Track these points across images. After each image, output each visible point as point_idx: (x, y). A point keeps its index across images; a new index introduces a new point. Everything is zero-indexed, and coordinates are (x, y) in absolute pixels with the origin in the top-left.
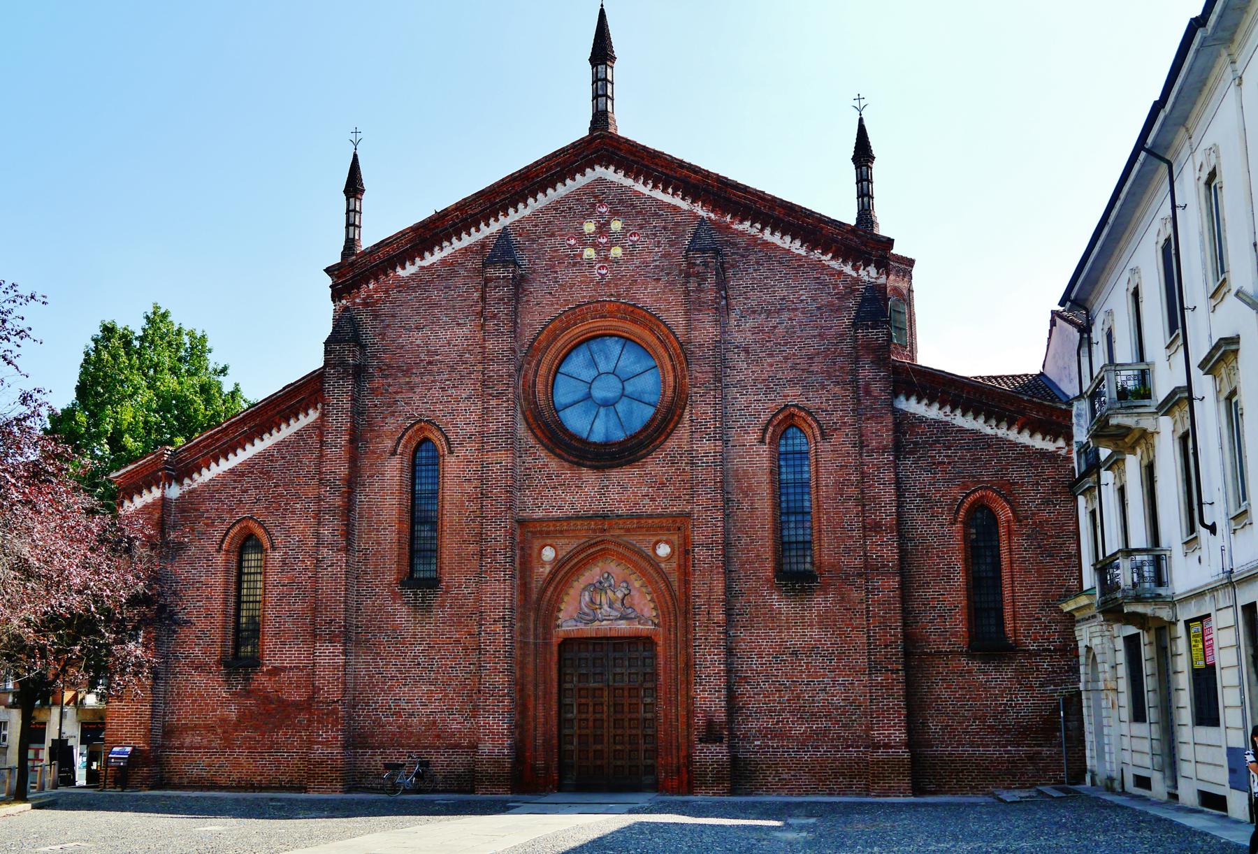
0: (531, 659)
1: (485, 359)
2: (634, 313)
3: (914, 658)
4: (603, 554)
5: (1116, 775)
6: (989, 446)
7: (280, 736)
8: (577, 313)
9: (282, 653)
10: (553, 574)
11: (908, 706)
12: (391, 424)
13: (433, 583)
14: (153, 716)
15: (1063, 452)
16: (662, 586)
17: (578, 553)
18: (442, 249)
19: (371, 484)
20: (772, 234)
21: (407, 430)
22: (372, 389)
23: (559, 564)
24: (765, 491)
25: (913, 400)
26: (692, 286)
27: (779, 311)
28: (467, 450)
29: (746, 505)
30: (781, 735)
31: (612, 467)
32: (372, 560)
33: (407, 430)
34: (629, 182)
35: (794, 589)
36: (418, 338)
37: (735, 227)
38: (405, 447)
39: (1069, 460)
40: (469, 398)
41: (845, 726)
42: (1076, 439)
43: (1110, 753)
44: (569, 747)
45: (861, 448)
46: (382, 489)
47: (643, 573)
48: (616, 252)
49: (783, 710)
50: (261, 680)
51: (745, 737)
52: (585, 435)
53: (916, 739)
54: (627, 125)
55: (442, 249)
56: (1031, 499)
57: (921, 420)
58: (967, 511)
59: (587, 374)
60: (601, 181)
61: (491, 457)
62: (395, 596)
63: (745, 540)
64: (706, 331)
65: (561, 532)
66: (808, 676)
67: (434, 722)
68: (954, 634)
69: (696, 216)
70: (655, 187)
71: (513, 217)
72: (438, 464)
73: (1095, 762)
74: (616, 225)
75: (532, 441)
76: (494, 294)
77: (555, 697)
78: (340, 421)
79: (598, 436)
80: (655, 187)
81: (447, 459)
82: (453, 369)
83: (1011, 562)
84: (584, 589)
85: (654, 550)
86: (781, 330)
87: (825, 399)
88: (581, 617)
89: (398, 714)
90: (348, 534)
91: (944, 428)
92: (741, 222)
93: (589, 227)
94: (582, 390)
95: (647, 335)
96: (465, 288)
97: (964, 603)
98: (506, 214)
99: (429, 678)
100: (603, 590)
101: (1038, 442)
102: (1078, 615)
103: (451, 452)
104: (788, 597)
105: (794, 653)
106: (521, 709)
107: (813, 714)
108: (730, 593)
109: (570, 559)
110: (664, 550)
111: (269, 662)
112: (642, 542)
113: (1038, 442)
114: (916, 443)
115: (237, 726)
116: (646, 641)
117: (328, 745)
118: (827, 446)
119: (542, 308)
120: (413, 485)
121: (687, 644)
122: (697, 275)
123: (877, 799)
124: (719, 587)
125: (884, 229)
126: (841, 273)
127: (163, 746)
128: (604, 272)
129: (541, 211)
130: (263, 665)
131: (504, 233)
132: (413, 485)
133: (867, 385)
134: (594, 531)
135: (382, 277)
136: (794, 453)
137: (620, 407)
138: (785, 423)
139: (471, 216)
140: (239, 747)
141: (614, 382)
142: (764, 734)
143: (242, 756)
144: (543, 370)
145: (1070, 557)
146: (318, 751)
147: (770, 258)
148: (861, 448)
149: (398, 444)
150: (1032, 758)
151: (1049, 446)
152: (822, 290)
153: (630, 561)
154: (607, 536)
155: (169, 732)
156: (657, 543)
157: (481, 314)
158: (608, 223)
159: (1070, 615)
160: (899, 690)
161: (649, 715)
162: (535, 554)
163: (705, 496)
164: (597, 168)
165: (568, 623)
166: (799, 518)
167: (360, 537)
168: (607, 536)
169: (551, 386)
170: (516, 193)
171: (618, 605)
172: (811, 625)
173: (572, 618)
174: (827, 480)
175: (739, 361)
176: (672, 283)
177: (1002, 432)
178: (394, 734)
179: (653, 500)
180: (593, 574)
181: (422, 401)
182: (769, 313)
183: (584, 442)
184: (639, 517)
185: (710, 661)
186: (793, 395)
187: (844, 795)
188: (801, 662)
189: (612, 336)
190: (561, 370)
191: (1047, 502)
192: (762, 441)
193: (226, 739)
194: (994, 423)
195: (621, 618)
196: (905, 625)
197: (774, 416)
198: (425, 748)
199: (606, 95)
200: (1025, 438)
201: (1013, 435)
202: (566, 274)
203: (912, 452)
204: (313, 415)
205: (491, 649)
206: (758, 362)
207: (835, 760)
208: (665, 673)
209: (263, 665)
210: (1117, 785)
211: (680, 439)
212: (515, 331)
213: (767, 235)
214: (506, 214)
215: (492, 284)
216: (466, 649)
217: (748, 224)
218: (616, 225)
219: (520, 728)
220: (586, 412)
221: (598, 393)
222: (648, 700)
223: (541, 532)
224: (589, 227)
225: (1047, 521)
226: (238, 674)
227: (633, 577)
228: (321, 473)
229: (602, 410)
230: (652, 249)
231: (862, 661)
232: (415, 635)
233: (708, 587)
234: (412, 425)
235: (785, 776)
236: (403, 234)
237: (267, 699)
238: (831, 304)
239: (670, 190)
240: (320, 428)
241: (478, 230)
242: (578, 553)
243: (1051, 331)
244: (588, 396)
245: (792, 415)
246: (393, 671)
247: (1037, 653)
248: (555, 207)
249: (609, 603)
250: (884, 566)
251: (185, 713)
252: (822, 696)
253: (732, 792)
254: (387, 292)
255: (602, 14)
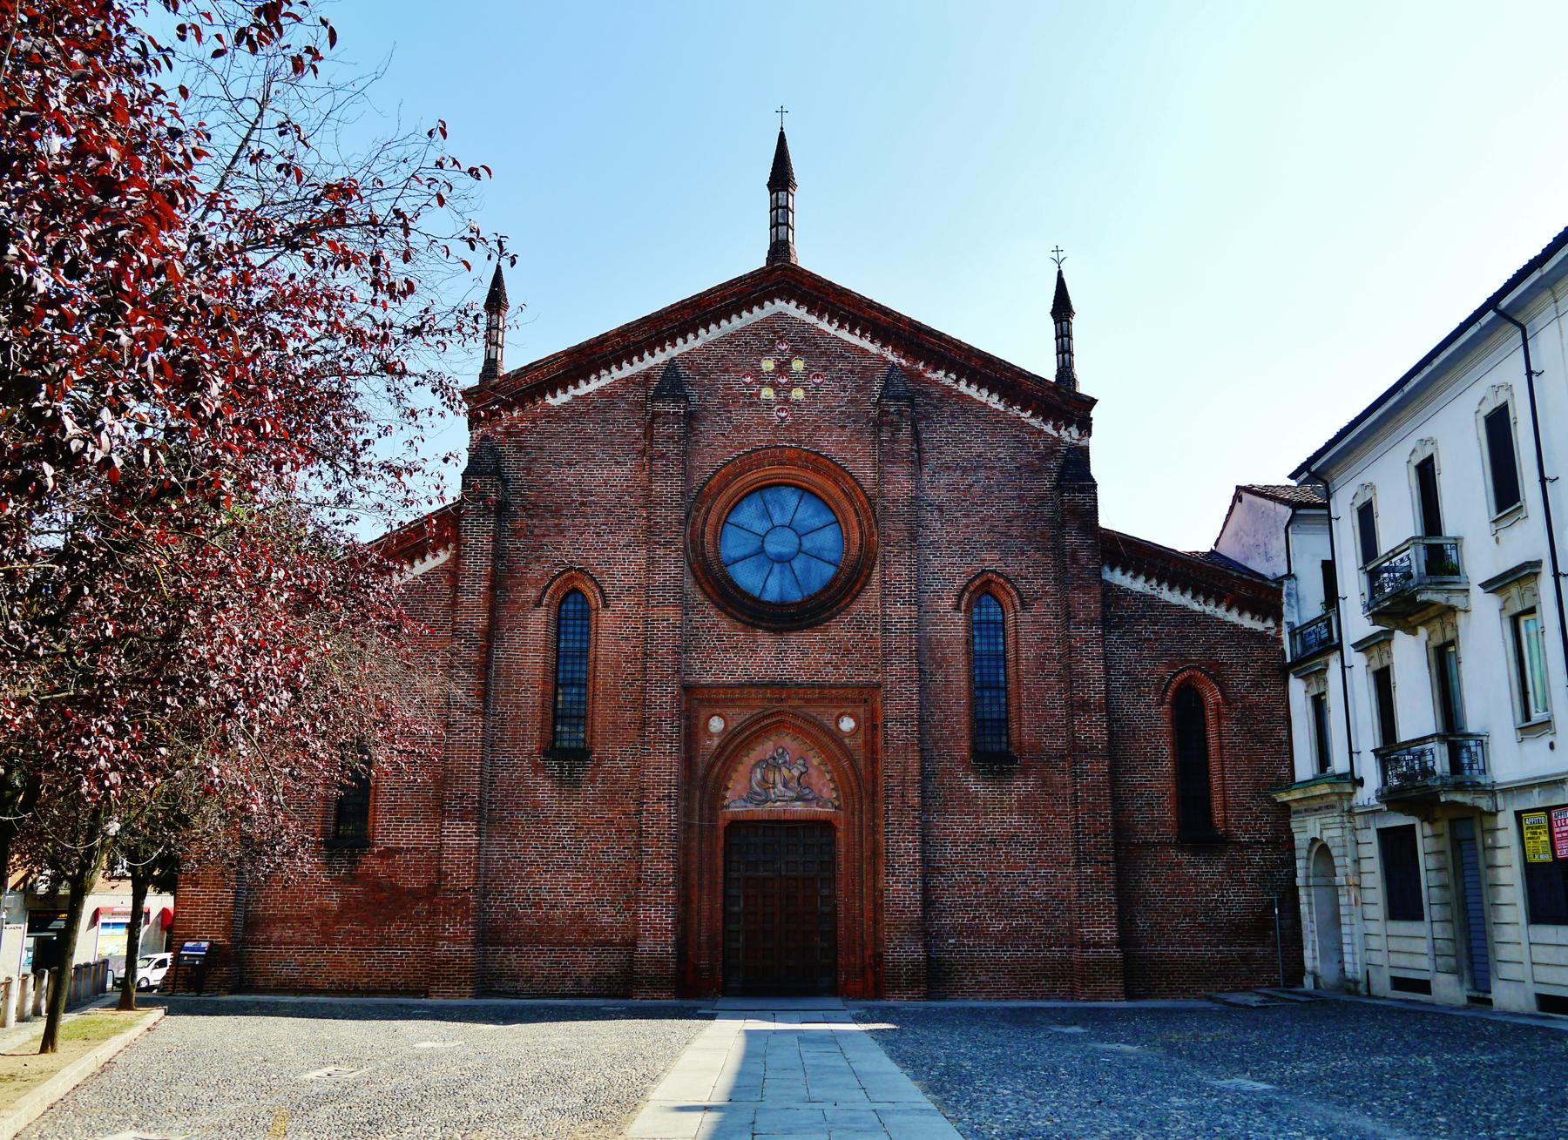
0: (695, 844)
1: (649, 501)
2: (817, 462)
3: (1125, 851)
4: (779, 726)
5: (1360, 976)
6: (1198, 624)
7: (393, 929)
8: (753, 459)
9: (397, 832)
10: (722, 748)
11: (1119, 902)
12: (536, 571)
13: (581, 754)
14: (236, 905)
15: (1272, 632)
16: (846, 764)
17: (751, 725)
18: (599, 378)
19: (511, 639)
20: (968, 385)
21: (555, 578)
22: (514, 530)
23: (729, 736)
24: (960, 663)
25: (1118, 572)
26: (885, 436)
27: (975, 469)
28: (623, 605)
29: (939, 678)
30: (978, 932)
31: (791, 630)
32: (509, 726)
33: (555, 578)
34: (812, 319)
35: (991, 771)
36: (569, 475)
37: (928, 375)
38: (552, 597)
39: (1279, 641)
40: (628, 546)
41: (1047, 922)
42: (1285, 619)
43: (1353, 953)
44: (735, 945)
45: (1068, 619)
46: (524, 644)
47: (823, 749)
48: (798, 394)
49: (980, 905)
50: (372, 864)
51: (939, 935)
52: (757, 593)
53: (1126, 940)
54: (806, 257)
55: (599, 378)
56: (1241, 681)
57: (1127, 593)
58: (1176, 692)
59: (760, 526)
60: (781, 315)
61: (656, 613)
62: (537, 768)
63: (938, 716)
64: (900, 484)
65: (732, 700)
66: (1007, 868)
67: (581, 915)
68: (1163, 824)
69: (886, 362)
70: (841, 326)
71: (680, 348)
72: (589, 619)
73: (1318, 963)
74: (798, 365)
75: (700, 597)
76: (661, 430)
77: (720, 889)
78: (478, 564)
79: (772, 592)
80: (841, 326)
81: (601, 613)
82: (610, 512)
83: (1221, 747)
84: (756, 765)
85: (837, 723)
86: (977, 489)
87: (1024, 567)
88: (751, 797)
89: (537, 905)
90: (484, 695)
91: (1150, 602)
92: (935, 371)
93: (768, 365)
94: (752, 544)
95: (830, 486)
96: (626, 423)
97: (1173, 790)
98: (674, 345)
99: (570, 861)
100: (777, 767)
101: (1247, 622)
102: (1294, 806)
103: (606, 606)
104: (985, 780)
105: (992, 842)
106: (684, 903)
107: (1012, 910)
108: (925, 776)
109: (743, 731)
110: (847, 724)
111: (382, 841)
112: (825, 715)
113: (1247, 622)
114: (1121, 617)
115: (341, 916)
116: (824, 827)
117: (455, 941)
118: (1026, 616)
119: (717, 448)
120: (558, 641)
121: (874, 830)
122: (891, 424)
123: (1088, 1004)
124: (914, 766)
125: (1084, 388)
126: (1041, 432)
127: (243, 940)
128: (783, 414)
129: (713, 343)
130: (374, 845)
131: (671, 364)
132: (558, 641)
133: (1074, 552)
134: (770, 700)
135: (529, 406)
136: (988, 622)
137: (796, 564)
138: (982, 589)
139: (634, 343)
140: (341, 943)
141: (790, 536)
142: (958, 931)
143: (343, 952)
144: (713, 518)
145: (1281, 743)
146: (444, 948)
147: (966, 411)
148: (1068, 619)
149: (544, 593)
150: (1245, 959)
151: (1258, 626)
152: (1021, 449)
153: (808, 735)
154: (784, 706)
155: (252, 924)
156: (840, 716)
157: (643, 453)
158: (789, 362)
159: (1285, 805)
160: (1110, 883)
161: (826, 909)
162: (701, 726)
163: (899, 666)
164: (777, 301)
165: (736, 804)
166: (994, 693)
167: (497, 699)
168: (784, 706)
169: (718, 536)
170: (686, 322)
171: (794, 784)
172: (1011, 811)
173: (741, 798)
174: (1028, 653)
175: (932, 519)
176: (860, 431)
177: (1210, 609)
178: (532, 928)
179: (837, 668)
180: (766, 748)
181: (568, 549)
182: (964, 470)
183: (757, 600)
184: (821, 687)
185: (904, 849)
186: (991, 560)
187: (1048, 999)
188: (998, 848)
189: (788, 485)
190: (731, 520)
191: (1256, 685)
192: (957, 608)
193: (324, 933)
194: (1201, 599)
195: (799, 799)
196: (1115, 814)
197: (971, 581)
198: (570, 945)
199: (787, 224)
200: (1233, 617)
201: (1220, 612)
202: (741, 416)
203: (1116, 627)
204: (443, 557)
205: (654, 831)
206: (953, 522)
207: (1038, 960)
208: (846, 861)
209: (374, 845)
210: (1362, 988)
211: (869, 601)
212: (687, 475)
213: (962, 386)
214: (674, 345)
215: (661, 420)
216: (620, 830)
217: (941, 373)
218: (798, 365)
219: (683, 922)
220: (759, 567)
221: (772, 548)
222: (825, 892)
223: (709, 700)
224: (768, 365)
225: (1257, 705)
226: (342, 855)
227: (811, 753)
228: (455, 623)
229: (777, 567)
230: (836, 393)
231: (1066, 851)
232: (559, 814)
233: (900, 767)
234: (561, 573)
235: (982, 978)
236: (555, 357)
237: (376, 886)
238: (1031, 464)
239: (858, 332)
240: (453, 572)
241: (641, 360)
242: (751, 725)
243: (1232, 508)
244: (761, 550)
245: (989, 581)
246: (533, 855)
247: (1248, 846)
248: (730, 339)
249: (781, 783)
250: (1093, 748)
251: (272, 903)
252: (1022, 889)
253: (928, 996)
254: (533, 421)
255: (782, 138)
